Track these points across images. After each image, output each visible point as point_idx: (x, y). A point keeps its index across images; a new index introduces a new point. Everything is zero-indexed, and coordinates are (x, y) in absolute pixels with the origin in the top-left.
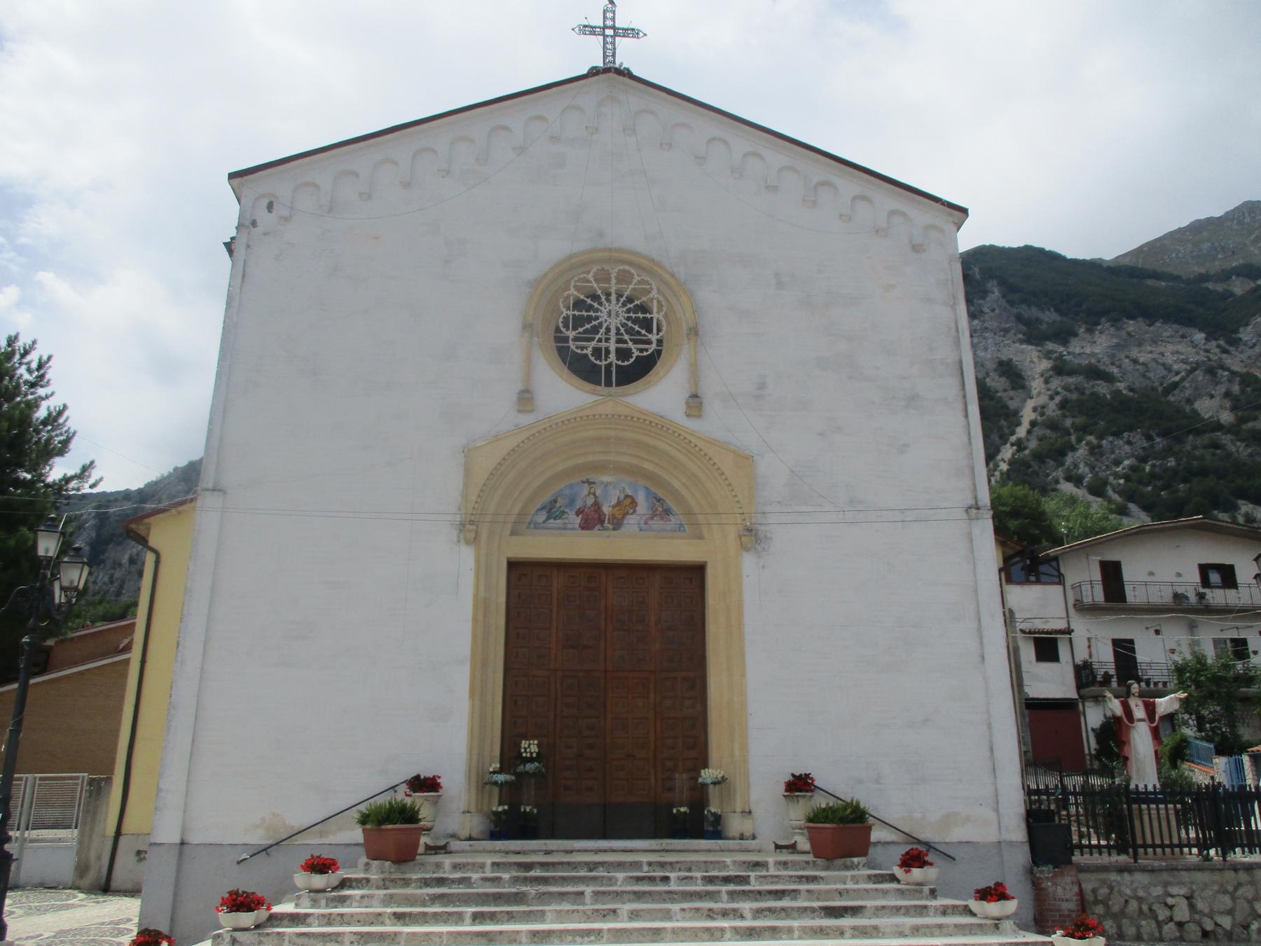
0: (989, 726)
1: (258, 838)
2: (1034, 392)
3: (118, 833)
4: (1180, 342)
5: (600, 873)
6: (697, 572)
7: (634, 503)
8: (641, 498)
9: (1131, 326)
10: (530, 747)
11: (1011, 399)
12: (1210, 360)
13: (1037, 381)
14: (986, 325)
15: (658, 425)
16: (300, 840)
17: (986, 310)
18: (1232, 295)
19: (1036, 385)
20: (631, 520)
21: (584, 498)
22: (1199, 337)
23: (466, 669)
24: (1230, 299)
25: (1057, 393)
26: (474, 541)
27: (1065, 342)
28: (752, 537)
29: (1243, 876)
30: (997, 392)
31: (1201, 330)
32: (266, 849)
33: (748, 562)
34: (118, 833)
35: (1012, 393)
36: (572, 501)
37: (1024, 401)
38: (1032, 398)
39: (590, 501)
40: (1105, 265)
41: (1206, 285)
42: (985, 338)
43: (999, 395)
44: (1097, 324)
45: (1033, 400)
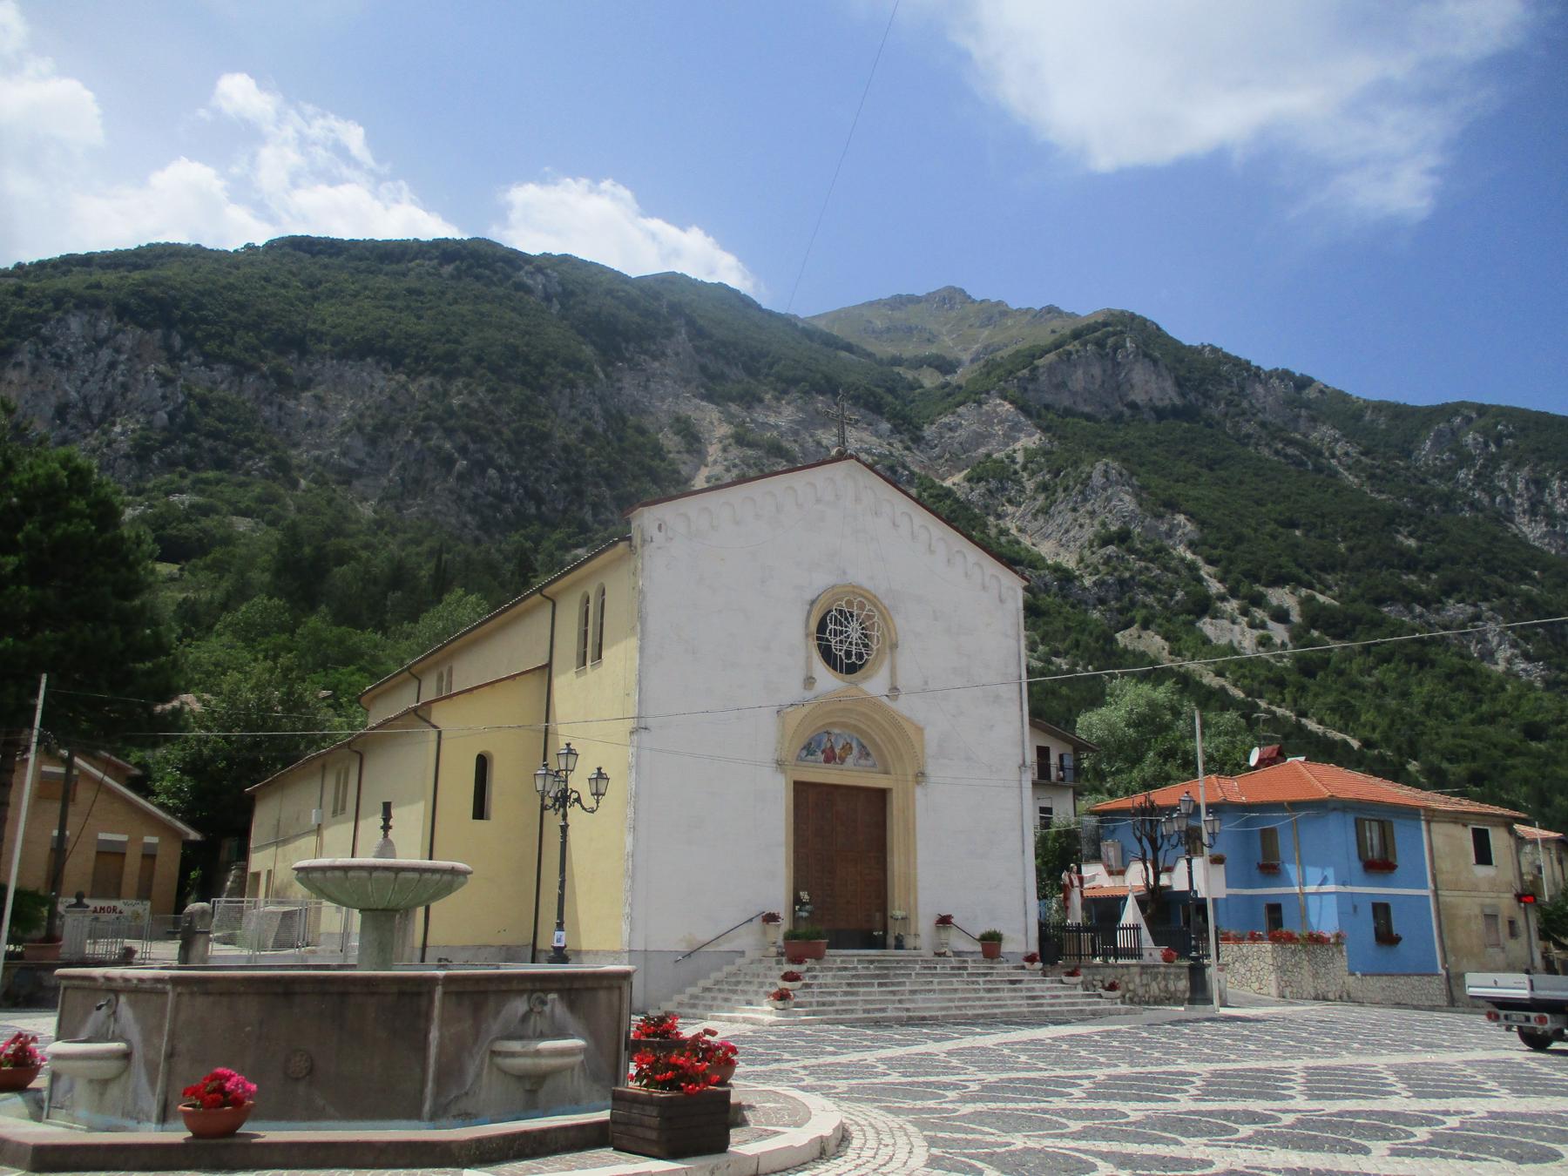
0: (1025, 890)
1: (683, 948)
2: (710, 459)
3: (424, 946)
4: (866, 429)
5: (902, 964)
6: (881, 795)
7: (851, 748)
8: (854, 745)
9: (821, 402)
10: (804, 896)
11: (684, 463)
12: (891, 454)
13: (715, 446)
14: (667, 370)
15: (873, 703)
16: (704, 949)
17: (669, 352)
18: (921, 387)
19: (714, 451)
20: (850, 760)
21: (826, 744)
22: (885, 426)
23: (783, 849)
24: (919, 391)
25: (735, 466)
26: (784, 772)
27: (749, 407)
28: (920, 776)
29: (1125, 970)
30: (669, 452)
31: (888, 420)
32: (689, 955)
33: (919, 792)
34: (424, 946)
35: (685, 457)
36: (819, 746)
37: (697, 469)
38: (706, 466)
39: (829, 745)
40: (800, 325)
41: (896, 369)
42: (663, 386)
43: (671, 456)
44: (785, 392)
45: (708, 469)
